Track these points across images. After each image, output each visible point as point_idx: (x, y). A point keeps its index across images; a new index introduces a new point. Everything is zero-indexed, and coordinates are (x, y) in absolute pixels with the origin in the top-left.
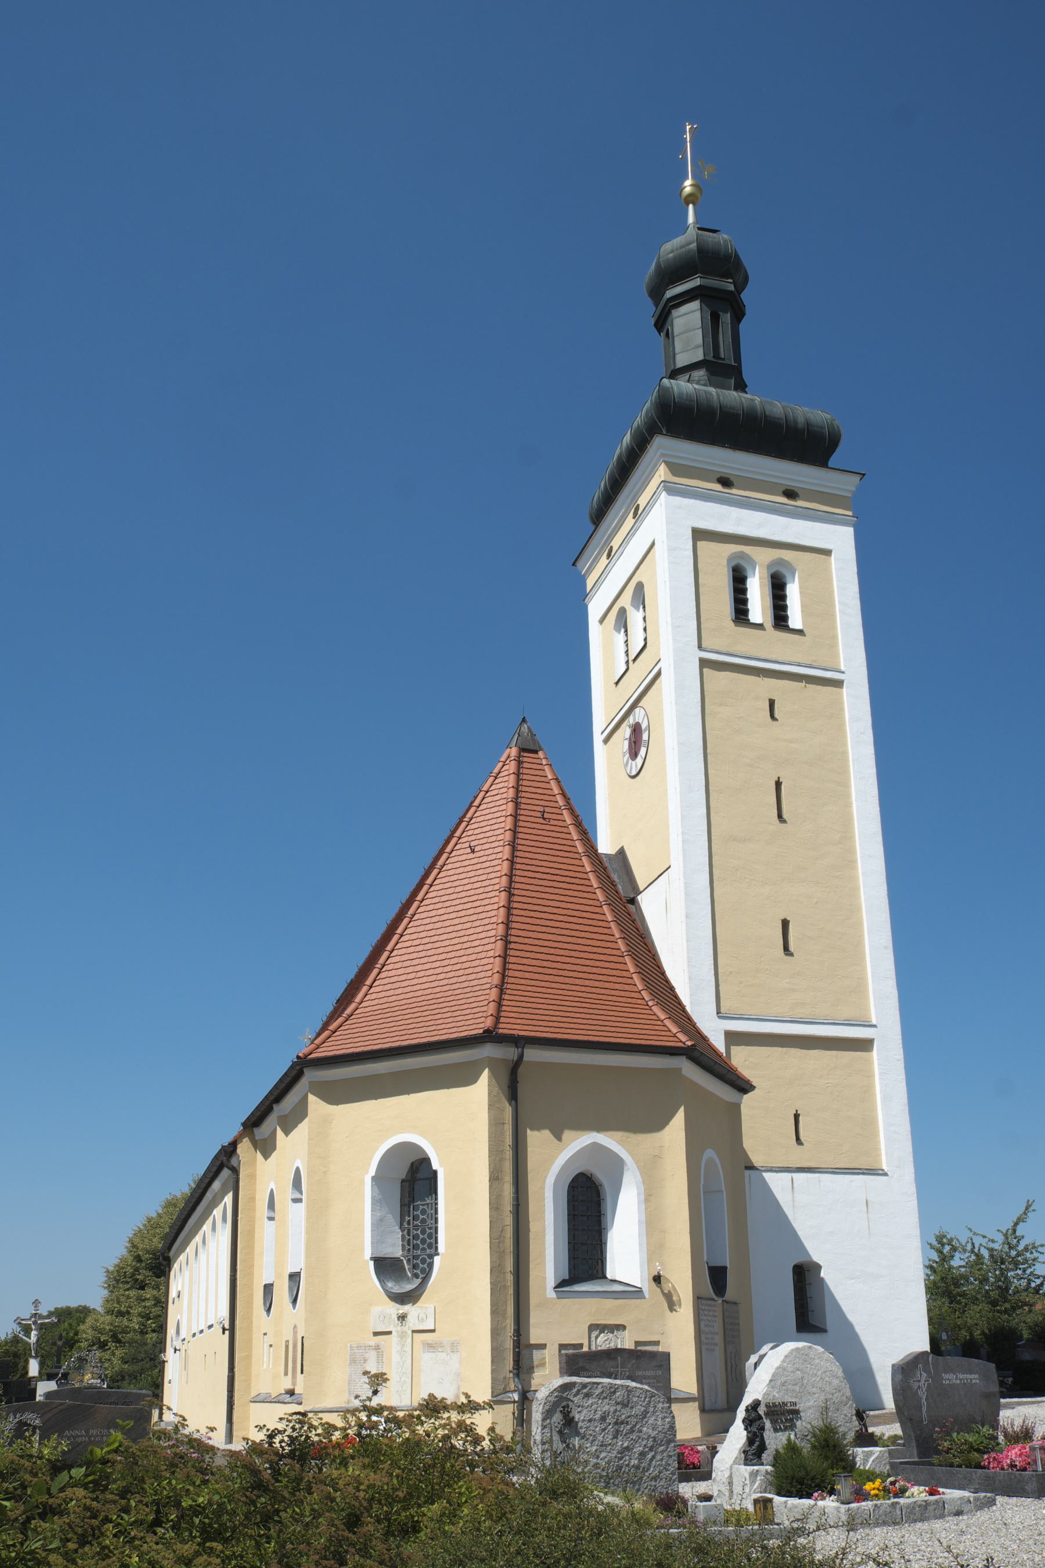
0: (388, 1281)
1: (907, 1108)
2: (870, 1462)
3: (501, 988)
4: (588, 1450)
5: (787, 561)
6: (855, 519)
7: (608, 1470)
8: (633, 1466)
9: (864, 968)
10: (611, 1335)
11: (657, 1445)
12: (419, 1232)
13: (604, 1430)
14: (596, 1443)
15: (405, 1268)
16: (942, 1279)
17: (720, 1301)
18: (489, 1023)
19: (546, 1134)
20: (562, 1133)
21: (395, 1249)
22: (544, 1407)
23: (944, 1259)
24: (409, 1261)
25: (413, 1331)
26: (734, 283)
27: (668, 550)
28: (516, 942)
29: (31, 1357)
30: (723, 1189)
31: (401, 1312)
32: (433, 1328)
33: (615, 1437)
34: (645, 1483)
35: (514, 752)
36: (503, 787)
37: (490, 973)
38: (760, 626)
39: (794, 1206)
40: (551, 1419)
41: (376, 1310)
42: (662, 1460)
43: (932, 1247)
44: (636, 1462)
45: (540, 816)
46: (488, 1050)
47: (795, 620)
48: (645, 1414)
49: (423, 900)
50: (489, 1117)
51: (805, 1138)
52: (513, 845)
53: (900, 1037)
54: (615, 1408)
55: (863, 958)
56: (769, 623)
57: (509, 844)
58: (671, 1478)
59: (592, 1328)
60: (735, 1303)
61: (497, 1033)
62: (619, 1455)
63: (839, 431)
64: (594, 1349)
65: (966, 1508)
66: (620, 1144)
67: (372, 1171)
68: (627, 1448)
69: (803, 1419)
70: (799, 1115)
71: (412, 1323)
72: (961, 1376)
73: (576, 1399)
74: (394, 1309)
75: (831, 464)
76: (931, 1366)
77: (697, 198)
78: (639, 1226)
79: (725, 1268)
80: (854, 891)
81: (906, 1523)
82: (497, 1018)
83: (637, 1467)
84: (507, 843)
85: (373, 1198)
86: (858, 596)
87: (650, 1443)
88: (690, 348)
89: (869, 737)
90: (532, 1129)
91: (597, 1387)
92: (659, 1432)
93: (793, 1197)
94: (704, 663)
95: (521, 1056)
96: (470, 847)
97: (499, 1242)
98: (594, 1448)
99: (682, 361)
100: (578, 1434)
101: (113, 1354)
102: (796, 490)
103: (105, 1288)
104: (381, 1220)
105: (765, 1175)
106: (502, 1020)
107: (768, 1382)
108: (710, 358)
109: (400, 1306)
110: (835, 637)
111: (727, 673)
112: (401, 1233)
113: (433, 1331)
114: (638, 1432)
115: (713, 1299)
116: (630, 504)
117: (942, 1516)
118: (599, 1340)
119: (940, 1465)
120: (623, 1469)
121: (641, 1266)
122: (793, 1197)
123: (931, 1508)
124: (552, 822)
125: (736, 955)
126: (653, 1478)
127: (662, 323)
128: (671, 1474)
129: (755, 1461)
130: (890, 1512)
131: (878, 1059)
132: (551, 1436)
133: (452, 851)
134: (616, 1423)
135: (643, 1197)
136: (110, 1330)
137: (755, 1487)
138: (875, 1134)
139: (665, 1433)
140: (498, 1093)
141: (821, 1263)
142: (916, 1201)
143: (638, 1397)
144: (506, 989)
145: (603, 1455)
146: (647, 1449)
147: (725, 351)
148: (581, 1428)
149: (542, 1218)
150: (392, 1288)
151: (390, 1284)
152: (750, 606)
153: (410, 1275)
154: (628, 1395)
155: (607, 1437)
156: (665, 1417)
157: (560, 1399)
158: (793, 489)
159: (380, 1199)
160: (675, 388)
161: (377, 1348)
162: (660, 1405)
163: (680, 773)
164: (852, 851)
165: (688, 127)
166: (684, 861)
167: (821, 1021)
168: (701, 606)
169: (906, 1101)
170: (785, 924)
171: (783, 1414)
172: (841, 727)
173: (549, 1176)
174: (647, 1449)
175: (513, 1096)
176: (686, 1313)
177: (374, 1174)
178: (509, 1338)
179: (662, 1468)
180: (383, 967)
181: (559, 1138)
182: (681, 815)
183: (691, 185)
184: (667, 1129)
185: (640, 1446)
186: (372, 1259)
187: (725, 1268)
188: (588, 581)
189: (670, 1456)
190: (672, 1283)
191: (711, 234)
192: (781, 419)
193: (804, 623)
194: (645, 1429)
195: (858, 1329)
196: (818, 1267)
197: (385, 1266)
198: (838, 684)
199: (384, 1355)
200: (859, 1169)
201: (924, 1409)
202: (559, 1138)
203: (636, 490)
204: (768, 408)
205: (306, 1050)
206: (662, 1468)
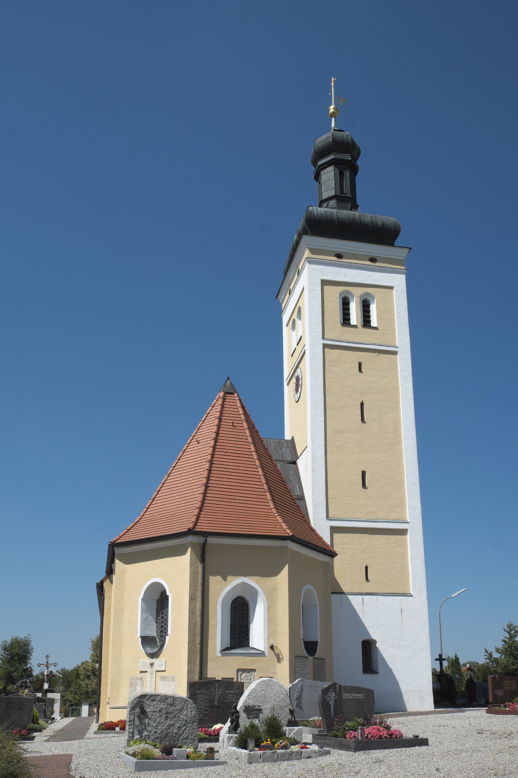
0: (147, 647)
1: (424, 563)
2: (292, 734)
3: (201, 509)
4: (152, 725)
5: (370, 294)
6: (406, 271)
7: (162, 734)
8: (175, 733)
9: (404, 494)
10: (248, 674)
11: (187, 723)
12: (163, 624)
13: (160, 716)
14: (156, 722)
15: (157, 642)
16: (509, 647)
17: (311, 658)
18: (191, 525)
19: (219, 578)
20: (227, 577)
21: (153, 632)
22: (131, 705)
23: (511, 637)
24: (159, 638)
25: (156, 671)
26: (352, 156)
27: (309, 291)
28: (212, 487)
29: (45, 682)
30: (317, 603)
31: (151, 662)
32: (164, 670)
33: (166, 719)
34: (180, 741)
35: (222, 394)
36: (215, 412)
37: (197, 502)
38: (355, 326)
39: (363, 612)
40: (134, 710)
41: (141, 661)
42: (189, 730)
43: (505, 630)
44: (176, 731)
45: (232, 425)
46: (191, 539)
47: (374, 322)
48: (182, 709)
49: (175, 466)
50: (190, 570)
51: (370, 579)
52: (216, 440)
53: (422, 528)
54: (166, 706)
55: (404, 489)
56: (360, 326)
57: (214, 439)
58: (194, 739)
59: (238, 670)
60: (323, 659)
61: (194, 531)
62: (168, 728)
63: (400, 227)
64: (239, 681)
65: (313, 755)
66: (255, 583)
67: (142, 596)
68: (172, 725)
69: (263, 713)
70: (368, 567)
71: (156, 667)
72: (354, 695)
73: (147, 702)
74: (149, 660)
75: (396, 243)
76: (338, 690)
77: (336, 114)
78: (264, 622)
79: (317, 642)
80: (400, 456)
81: (280, 761)
82: (196, 523)
83: (177, 733)
84: (213, 439)
85: (142, 608)
86: (407, 308)
87: (184, 723)
88: (329, 189)
89: (410, 379)
90: (212, 576)
91: (158, 697)
92: (189, 718)
93: (363, 608)
94: (325, 346)
95: (206, 541)
96: (197, 441)
97: (193, 629)
98: (155, 724)
99: (325, 196)
100: (147, 717)
101: (93, 682)
102: (376, 258)
103: (92, 650)
104: (146, 619)
105: (349, 596)
106: (198, 524)
107: (247, 696)
108: (338, 194)
109: (151, 659)
110: (394, 330)
111: (337, 350)
112: (156, 625)
113: (165, 671)
114: (178, 717)
115: (307, 657)
116: (296, 270)
117: (300, 758)
118: (242, 676)
119: (331, 736)
120: (169, 734)
121: (265, 641)
122: (363, 608)
123: (294, 755)
124: (237, 428)
125: (337, 489)
126: (185, 738)
127: (317, 177)
128: (194, 737)
129: (232, 732)
130: (271, 756)
131: (410, 539)
132: (134, 718)
133: (190, 443)
134: (167, 713)
135: (266, 608)
136: (92, 670)
137: (230, 744)
138: (407, 576)
139: (192, 718)
140: (195, 559)
141: (376, 640)
142: (427, 609)
143: (179, 701)
144: (204, 509)
145: (159, 727)
146: (182, 725)
147: (347, 190)
148: (149, 715)
149: (215, 618)
150: (148, 651)
151: (148, 649)
152: (351, 316)
153: (159, 644)
154: (174, 701)
155: (162, 720)
156: (192, 711)
157: (140, 702)
158: (374, 257)
159: (146, 609)
160: (315, 211)
161: (141, 679)
162: (190, 706)
163: (311, 401)
164: (400, 436)
165: (333, 79)
166: (312, 444)
167: (381, 521)
168: (325, 318)
169: (424, 560)
170: (364, 474)
171: (253, 711)
172: (396, 374)
173: (220, 598)
174: (182, 725)
175: (203, 560)
176: (285, 664)
177: (142, 597)
178: (197, 675)
179: (189, 734)
180: (154, 499)
181: (225, 580)
182: (311, 421)
183: (333, 108)
184: (280, 575)
185: (179, 724)
186: (140, 637)
187: (316, 643)
188: (283, 305)
189: (194, 729)
190: (279, 649)
191: (340, 132)
192: (370, 223)
193: (378, 324)
194: (181, 716)
195: (394, 672)
196: (375, 642)
197: (146, 641)
198: (395, 353)
199: (144, 683)
200: (398, 593)
201: (332, 710)
202: (225, 580)
203: (298, 261)
204: (362, 218)
205: (114, 539)
206: (189, 734)
